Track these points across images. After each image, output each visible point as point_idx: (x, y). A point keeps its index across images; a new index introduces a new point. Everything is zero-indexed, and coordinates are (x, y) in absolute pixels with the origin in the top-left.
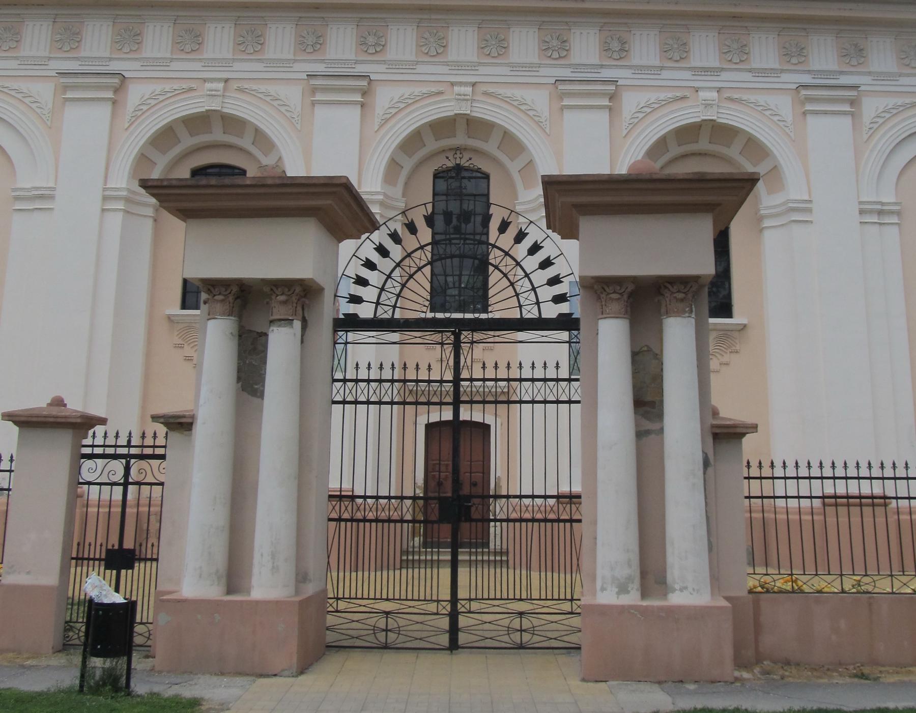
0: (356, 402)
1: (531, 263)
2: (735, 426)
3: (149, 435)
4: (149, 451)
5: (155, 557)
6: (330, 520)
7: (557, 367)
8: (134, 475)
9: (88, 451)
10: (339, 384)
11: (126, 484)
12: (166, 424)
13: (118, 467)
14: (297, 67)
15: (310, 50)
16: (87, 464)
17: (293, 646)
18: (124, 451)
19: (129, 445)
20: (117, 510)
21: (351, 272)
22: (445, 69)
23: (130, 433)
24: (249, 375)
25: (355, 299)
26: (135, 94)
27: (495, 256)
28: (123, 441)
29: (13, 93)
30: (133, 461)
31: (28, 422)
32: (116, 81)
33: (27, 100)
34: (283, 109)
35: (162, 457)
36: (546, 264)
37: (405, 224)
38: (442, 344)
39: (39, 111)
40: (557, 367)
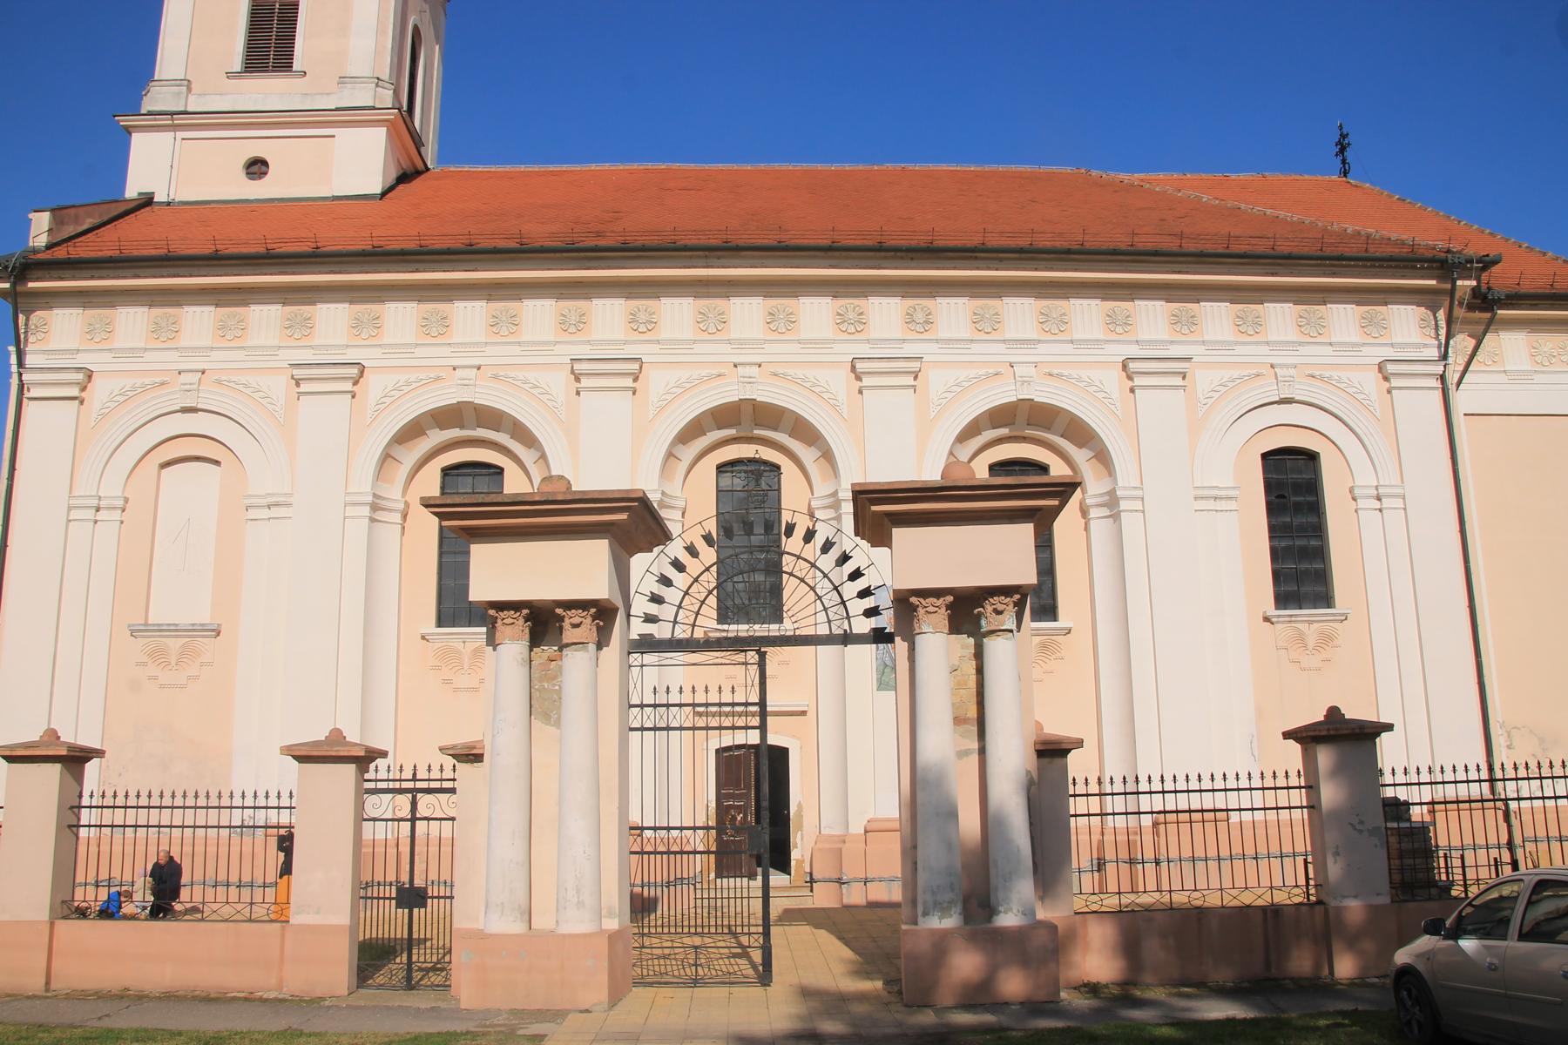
1: (827, 562)
2: (1059, 742)
8: (422, 811)
9: (371, 785)
11: (413, 820)
13: (404, 801)
14: (559, 349)
16: (371, 800)
18: (410, 785)
19: (414, 779)
20: (405, 849)
22: (726, 348)
24: (542, 703)
25: (650, 619)
26: (375, 385)
27: (788, 563)
31: (306, 756)
32: (355, 371)
33: (256, 396)
35: (453, 791)
36: (856, 575)
38: (746, 664)
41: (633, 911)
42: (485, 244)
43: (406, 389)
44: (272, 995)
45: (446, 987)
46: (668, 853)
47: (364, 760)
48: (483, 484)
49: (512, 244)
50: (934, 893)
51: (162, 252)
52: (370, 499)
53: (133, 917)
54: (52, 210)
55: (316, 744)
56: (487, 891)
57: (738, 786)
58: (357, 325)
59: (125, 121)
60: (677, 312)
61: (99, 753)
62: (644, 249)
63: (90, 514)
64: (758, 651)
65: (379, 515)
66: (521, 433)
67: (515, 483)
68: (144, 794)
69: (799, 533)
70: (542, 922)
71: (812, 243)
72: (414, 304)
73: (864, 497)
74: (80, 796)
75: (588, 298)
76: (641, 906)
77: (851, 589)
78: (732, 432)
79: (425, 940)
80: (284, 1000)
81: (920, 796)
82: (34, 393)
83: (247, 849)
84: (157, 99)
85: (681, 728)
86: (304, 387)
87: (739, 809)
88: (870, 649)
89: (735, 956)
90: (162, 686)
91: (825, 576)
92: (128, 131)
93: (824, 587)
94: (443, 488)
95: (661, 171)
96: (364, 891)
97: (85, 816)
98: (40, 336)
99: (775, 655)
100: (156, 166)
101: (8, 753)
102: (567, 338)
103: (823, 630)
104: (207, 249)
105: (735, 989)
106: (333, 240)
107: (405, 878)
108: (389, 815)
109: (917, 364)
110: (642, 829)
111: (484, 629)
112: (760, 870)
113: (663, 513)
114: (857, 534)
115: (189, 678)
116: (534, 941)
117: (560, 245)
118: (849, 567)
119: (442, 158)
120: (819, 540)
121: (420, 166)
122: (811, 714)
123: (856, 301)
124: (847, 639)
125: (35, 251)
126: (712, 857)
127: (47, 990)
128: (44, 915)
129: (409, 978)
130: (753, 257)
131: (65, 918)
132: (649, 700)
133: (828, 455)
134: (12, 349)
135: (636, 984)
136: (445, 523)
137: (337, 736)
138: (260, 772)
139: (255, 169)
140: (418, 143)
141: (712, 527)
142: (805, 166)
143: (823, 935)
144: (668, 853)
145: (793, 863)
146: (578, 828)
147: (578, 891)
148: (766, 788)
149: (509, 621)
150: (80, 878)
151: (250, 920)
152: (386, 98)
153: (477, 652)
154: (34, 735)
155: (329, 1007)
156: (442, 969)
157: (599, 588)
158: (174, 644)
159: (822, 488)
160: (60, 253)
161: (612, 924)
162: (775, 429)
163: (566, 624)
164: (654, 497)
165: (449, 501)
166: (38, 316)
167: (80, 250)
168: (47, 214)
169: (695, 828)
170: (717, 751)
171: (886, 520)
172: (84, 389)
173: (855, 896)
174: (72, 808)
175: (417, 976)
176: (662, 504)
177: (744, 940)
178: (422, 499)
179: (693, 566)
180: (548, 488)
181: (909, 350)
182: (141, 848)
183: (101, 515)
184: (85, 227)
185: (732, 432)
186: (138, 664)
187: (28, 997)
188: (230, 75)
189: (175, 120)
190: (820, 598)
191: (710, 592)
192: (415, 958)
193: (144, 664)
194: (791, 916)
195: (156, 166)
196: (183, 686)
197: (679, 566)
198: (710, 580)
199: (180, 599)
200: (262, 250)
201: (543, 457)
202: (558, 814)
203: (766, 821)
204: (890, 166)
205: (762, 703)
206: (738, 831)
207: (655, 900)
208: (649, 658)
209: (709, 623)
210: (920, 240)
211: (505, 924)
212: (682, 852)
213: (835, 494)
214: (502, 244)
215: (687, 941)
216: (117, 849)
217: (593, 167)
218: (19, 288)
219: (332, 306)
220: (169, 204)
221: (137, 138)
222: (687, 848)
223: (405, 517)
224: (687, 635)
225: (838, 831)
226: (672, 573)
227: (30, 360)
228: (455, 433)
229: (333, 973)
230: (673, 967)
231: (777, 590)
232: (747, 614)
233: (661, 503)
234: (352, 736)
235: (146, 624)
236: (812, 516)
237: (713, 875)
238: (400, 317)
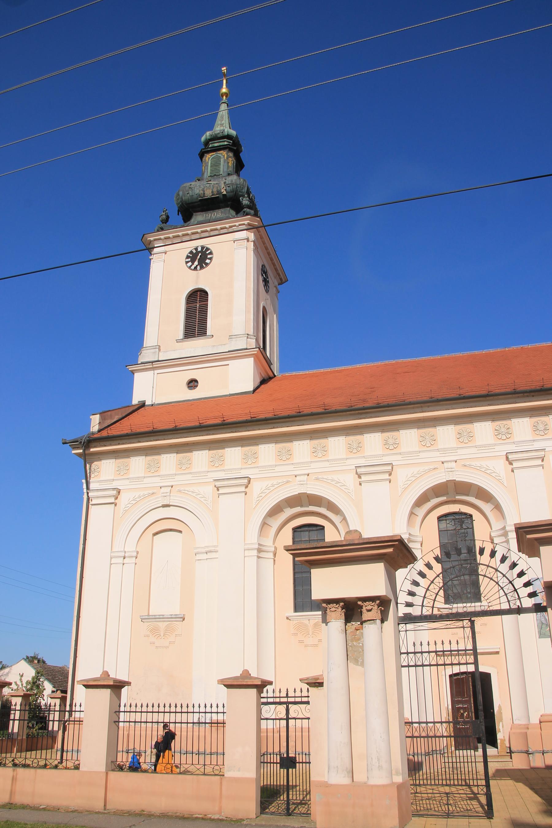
0: (423, 665)
3: (298, 691)
4: (298, 700)
5: (308, 761)
6: (407, 737)
8: (292, 714)
9: (264, 700)
10: (404, 656)
12: (307, 684)
13: (282, 709)
14: (349, 462)
15: (355, 451)
16: (265, 708)
17: (395, 812)
18: (285, 700)
19: (287, 696)
23: (287, 690)
24: (353, 653)
25: (409, 605)
26: (256, 488)
27: (482, 570)
28: (283, 694)
29: (190, 493)
30: (290, 705)
31: (231, 685)
32: (246, 481)
33: (198, 497)
34: (343, 488)
35: (308, 703)
36: (521, 574)
37: (434, 558)
38: (463, 627)
39: (205, 502)
41: (409, 770)
42: (307, 411)
43: (272, 488)
44: (216, 817)
45: (308, 814)
46: (428, 737)
47: (260, 687)
48: (314, 535)
49: (320, 410)
51: (151, 429)
52: (257, 546)
53: (146, 771)
54: (100, 414)
55: (236, 678)
56: (329, 759)
57: (463, 696)
58: (246, 458)
59: (131, 368)
60: (409, 438)
61: (128, 683)
62: (388, 406)
63: (121, 560)
64: (470, 620)
65: (262, 555)
66: (332, 507)
67: (331, 535)
68: (150, 705)
69: (487, 552)
70: (359, 777)
71: (478, 393)
72: (273, 445)
73: (522, 531)
74: (120, 706)
76: (414, 767)
77: (519, 583)
78: (444, 498)
79: (296, 786)
80: (222, 820)
82: (94, 502)
83: (202, 734)
84: (146, 356)
85: (430, 665)
86: (222, 491)
87: (465, 709)
88: (532, 616)
89: (470, 799)
90: (157, 647)
91: (504, 576)
92: (133, 372)
93: (503, 582)
94: (293, 539)
95: (392, 365)
96: (262, 759)
97: (122, 717)
98: (96, 474)
99: (479, 621)
100: (149, 388)
101: (86, 683)
102: (352, 455)
103: (505, 606)
104: (171, 426)
105: (472, 820)
106: (232, 416)
107: (284, 750)
108: (273, 717)
109: (543, 453)
110: (412, 723)
111: (320, 613)
112: (480, 745)
113: (411, 545)
114: (519, 551)
115: (170, 643)
116: (356, 789)
117: (345, 408)
118: (517, 570)
119: (281, 370)
120: (498, 556)
121: (271, 375)
122: (502, 653)
123: (504, 422)
124: (519, 611)
125: (93, 433)
126: (453, 739)
127: (105, 809)
128: (103, 769)
129: (288, 809)
130: (446, 405)
131: (113, 770)
132: (411, 649)
133: (498, 507)
134: (84, 481)
135: (414, 815)
136: (297, 559)
137: (246, 674)
138: (206, 692)
139: (192, 384)
140: (269, 363)
141: (438, 552)
142: (469, 353)
143: (520, 786)
144: (428, 737)
145: (499, 741)
146: (377, 723)
147: (378, 760)
148: (480, 698)
149: (333, 609)
150: (120, 748)
151: (204, 774)
152: (252, 343)
153: (316, 625)
154: (98, 674)
155: (246, 825)
156: (305, 804)
157: (380, 589)
158: (162, 625)
159: (497, 525)
160: (104, 434)
161: (399, 779)
162: (468, 495)
163: (364, 610)
164: (405, 537)
165: (299, 547)
166: (95, 464)
167: (115, 431)
168: (98, 415)
169: (441, 722)
170: (450, 676)
171: (536, 542)
172: (116, 498)
173: (538, 762)
174: (116, 712)
175: (292, 807)
176: (410, 540)
177: (475, 789)
178: (284, 546)
179: (430, 575)
180: (350, 537)
181: (538, 445)
182: (149, 732)
183: (126, 561)
184: (115, 420)
185: (444, 498)
186: (145, 636)
187: (96, 813)
188: (178, 341)
189: (154, 365)
190: (502, 588)
191: (440, 588)
192: (291, 796)
193: (148, 636)
194: (502, 774)
195: (149, 388)
196: (167, 647)
197: (422, 575)
198: (439, 582)
199: (165, 603)
200: (197, 424)
201: (345, 519)
202: (365, 717)
203: (482, 718)
204: (515, 347)
205: (475, 649)
206: (465, 723)
208: (410, 626)
209: (441, 606)
210: (535, 385)
211: (338, 778)
212: (435, 737)
213: (504, 528)
214: (315, 410)
215: (442, 789)
216: (138, 733)
217: (358, 366)
218: (87, 452)
219: (233, 449)
220: (152, 405)
221: (136, 375)
222: (438, 734)
223: (275, 555)
224: (429, 613)
225: (523, 722)
226: (419, 579)
227: (92, 486)
228: (298, 509)
229: (247, 805)
230: (434, 805)
231: (476, 585)
232: (461, 598)
233: (409, 540)
234: (254, 674)
235: (148, 615)
236: (492, 542)
237: (453, 748)
238: (267, 452)
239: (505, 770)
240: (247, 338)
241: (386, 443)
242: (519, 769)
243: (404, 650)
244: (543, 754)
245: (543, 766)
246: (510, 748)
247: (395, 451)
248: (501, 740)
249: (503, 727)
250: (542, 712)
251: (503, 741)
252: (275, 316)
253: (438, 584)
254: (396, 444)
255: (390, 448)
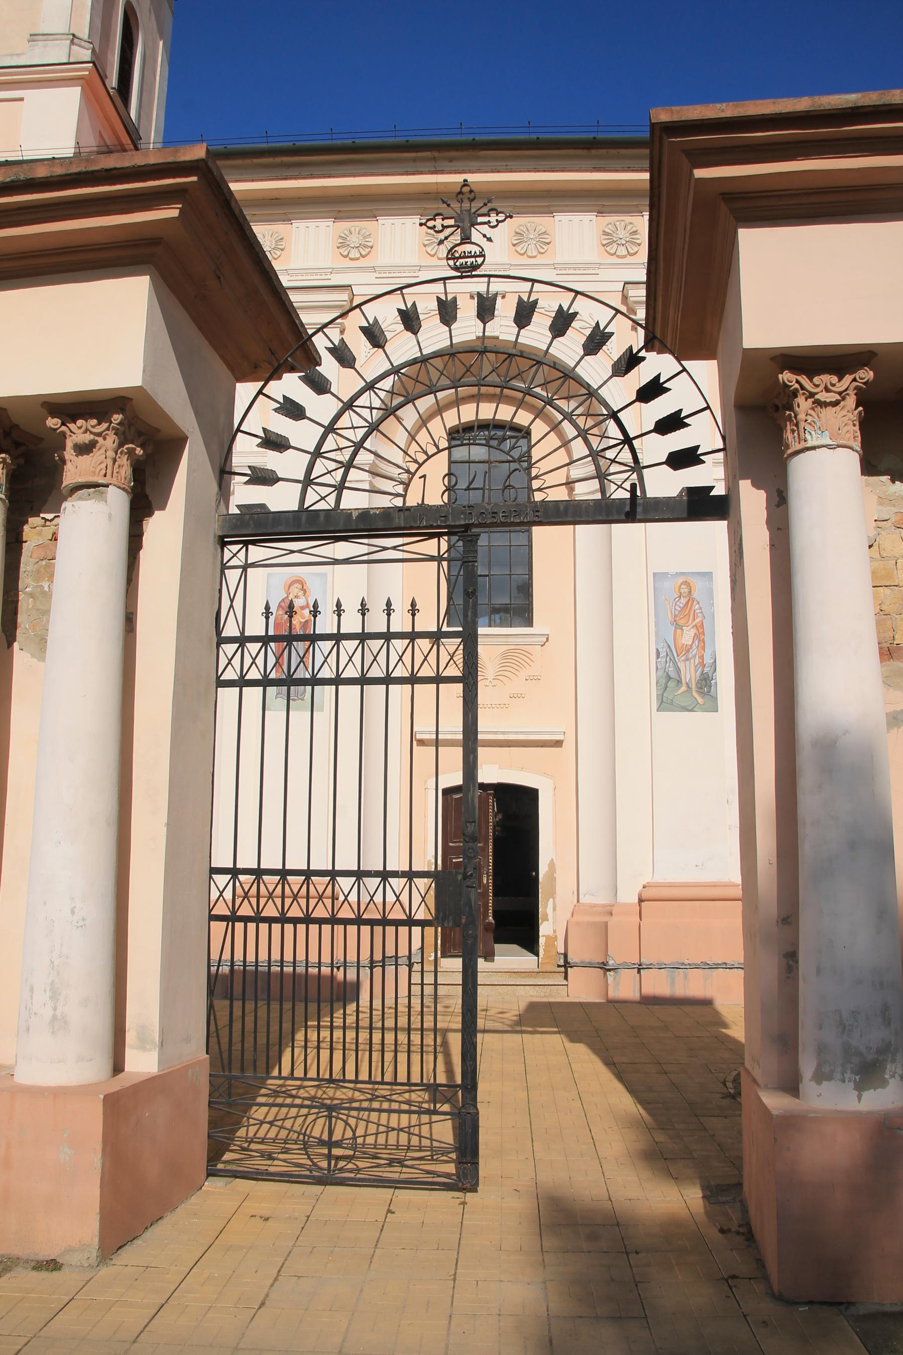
1: (620, 391)
6: (213, 918)
7: (413, 610)
21: (254, 424)
25: (262, 477)
40: (413, 610)
50: (843, 1028)
75: (287, 219)
81: (808, 803)
103: (587, 491)
122: (569, 745)
123: (628, 219)
124: (637, 509)
143: (581, 1051)
145: (542, 941)
147: (55, 995)
173: (625, 987)
207: (358, 984)
225: (602, 899)
239: (550, 1004)
240: (72, 42)
241: (343, 243)
242: (581, 1004)
243: (231, 630)
244: (639, 972)
245: (636, 996)
246: (565, 955)
247: (361, 263)
248: (548, 937)
249: (554, 909)
250: (647, 879)
251: (552, 940)
252: (161, 43)
253: (366, 413)
254: (366, 247)
255: (351, 256)
